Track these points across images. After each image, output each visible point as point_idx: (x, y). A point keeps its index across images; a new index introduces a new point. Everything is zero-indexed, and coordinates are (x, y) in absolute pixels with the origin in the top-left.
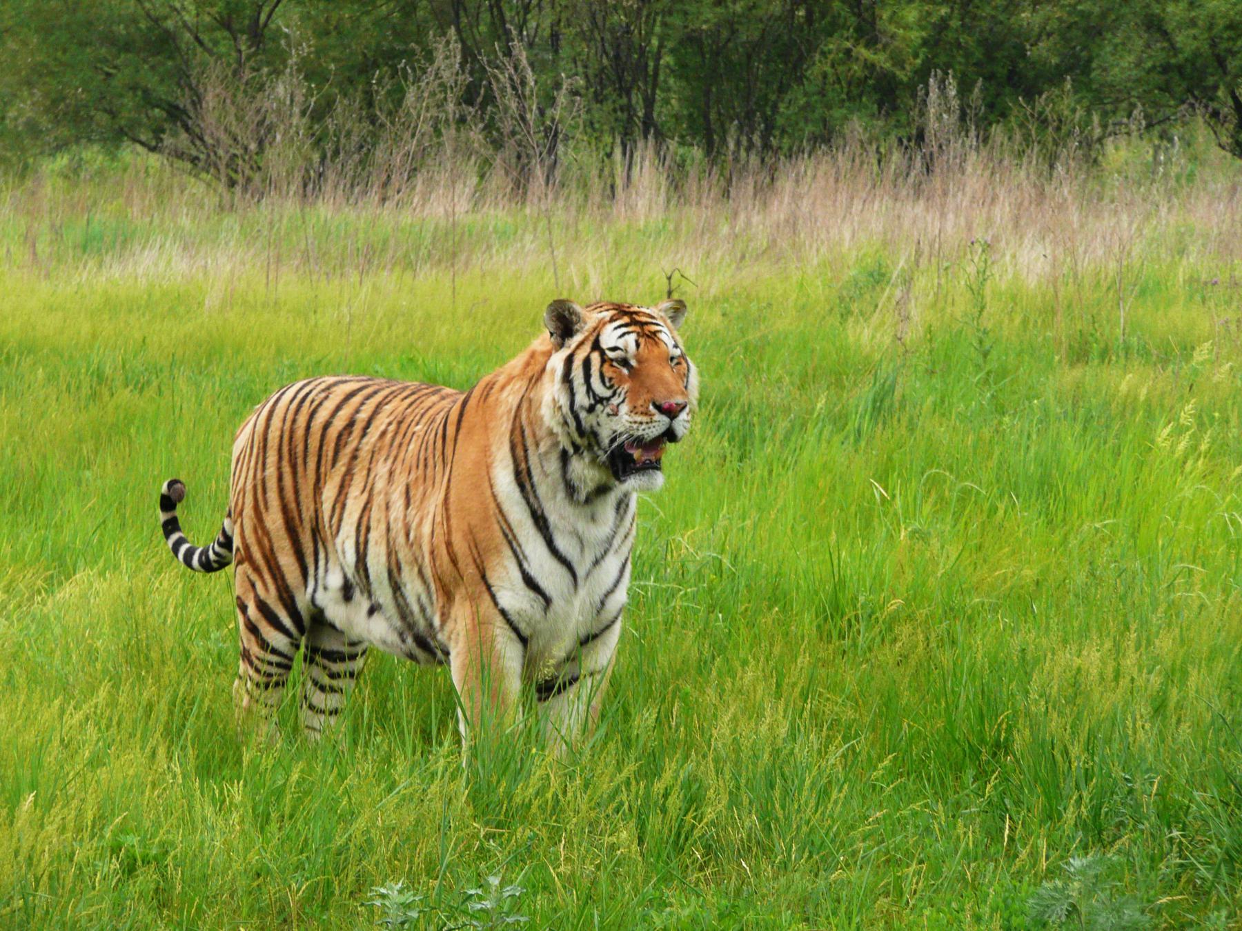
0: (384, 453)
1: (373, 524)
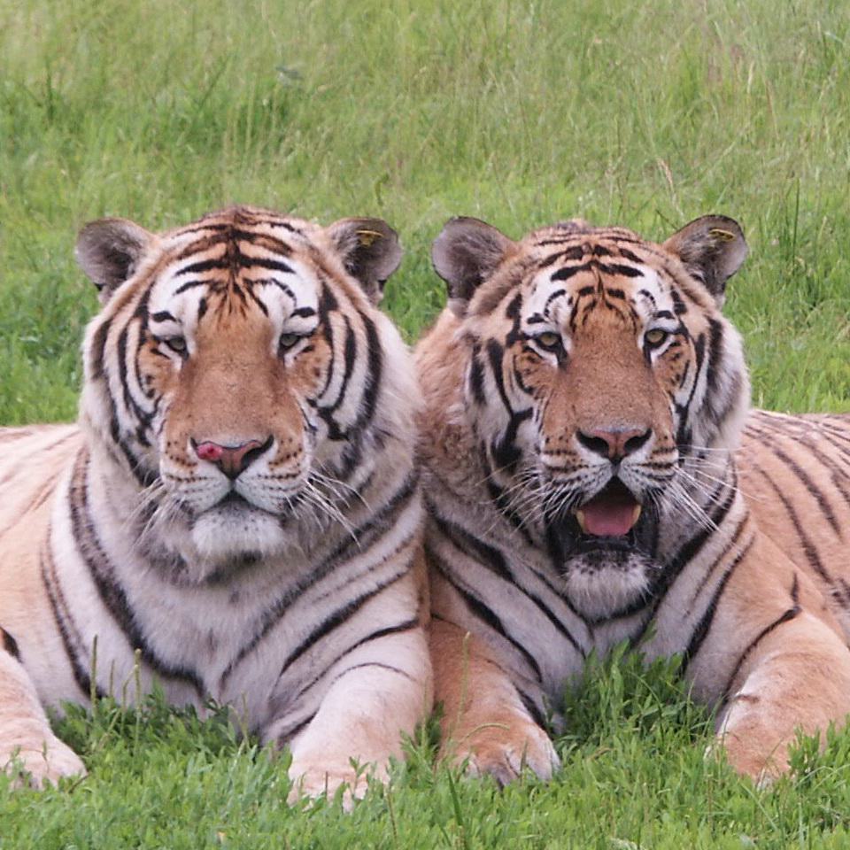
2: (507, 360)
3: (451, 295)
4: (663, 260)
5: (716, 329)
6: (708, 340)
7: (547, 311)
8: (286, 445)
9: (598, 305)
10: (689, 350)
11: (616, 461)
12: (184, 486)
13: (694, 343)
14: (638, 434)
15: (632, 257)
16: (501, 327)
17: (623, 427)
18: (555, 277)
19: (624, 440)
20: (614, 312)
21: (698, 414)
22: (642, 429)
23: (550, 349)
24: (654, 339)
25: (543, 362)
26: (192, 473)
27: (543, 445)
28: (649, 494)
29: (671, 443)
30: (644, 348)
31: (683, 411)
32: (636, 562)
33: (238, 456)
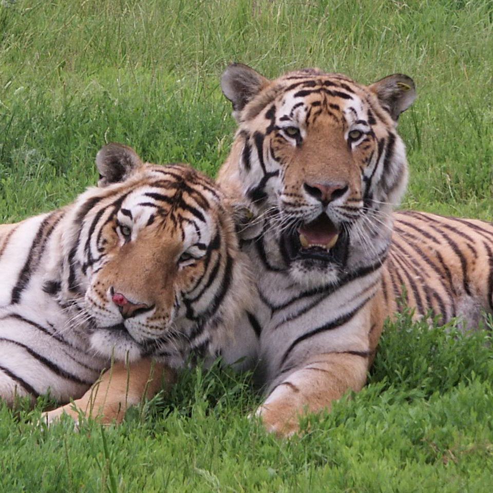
2: (266, 142)
3: (234, 109)
4: (367, 95)
5: (392, 139)
6: (386, 142)
7: (292, 114)
8: (159, 312)
9: (323, 112)
10: (375, 146)
11: (325, 203)
12: (96, 309)
13: (378, 142)
14: (340, 187)
15: (348, 89)
16: (262, 124)
17: (331, 183)
18: (296, 96)
19: (331, 190)
20: (332, 117)
21: (377, 185)
22: (342, 184)
23: (292, 136)
24: (354, 136)
25: (287, 143)
26: (104, 305)
27: (283, 190)
28: (342, 225)
29: (359, 196)
30: (348, 140)
31: (368, 181)
32: (333, 268)
33: (132, 308)
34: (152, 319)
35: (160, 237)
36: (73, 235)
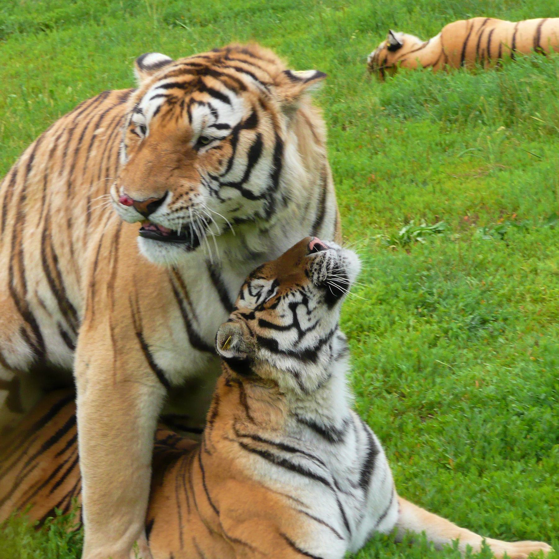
0: (57, 169)
1: (58, 252)
34: (174, 203)
35: (164, 126)
36: (63, 365)
